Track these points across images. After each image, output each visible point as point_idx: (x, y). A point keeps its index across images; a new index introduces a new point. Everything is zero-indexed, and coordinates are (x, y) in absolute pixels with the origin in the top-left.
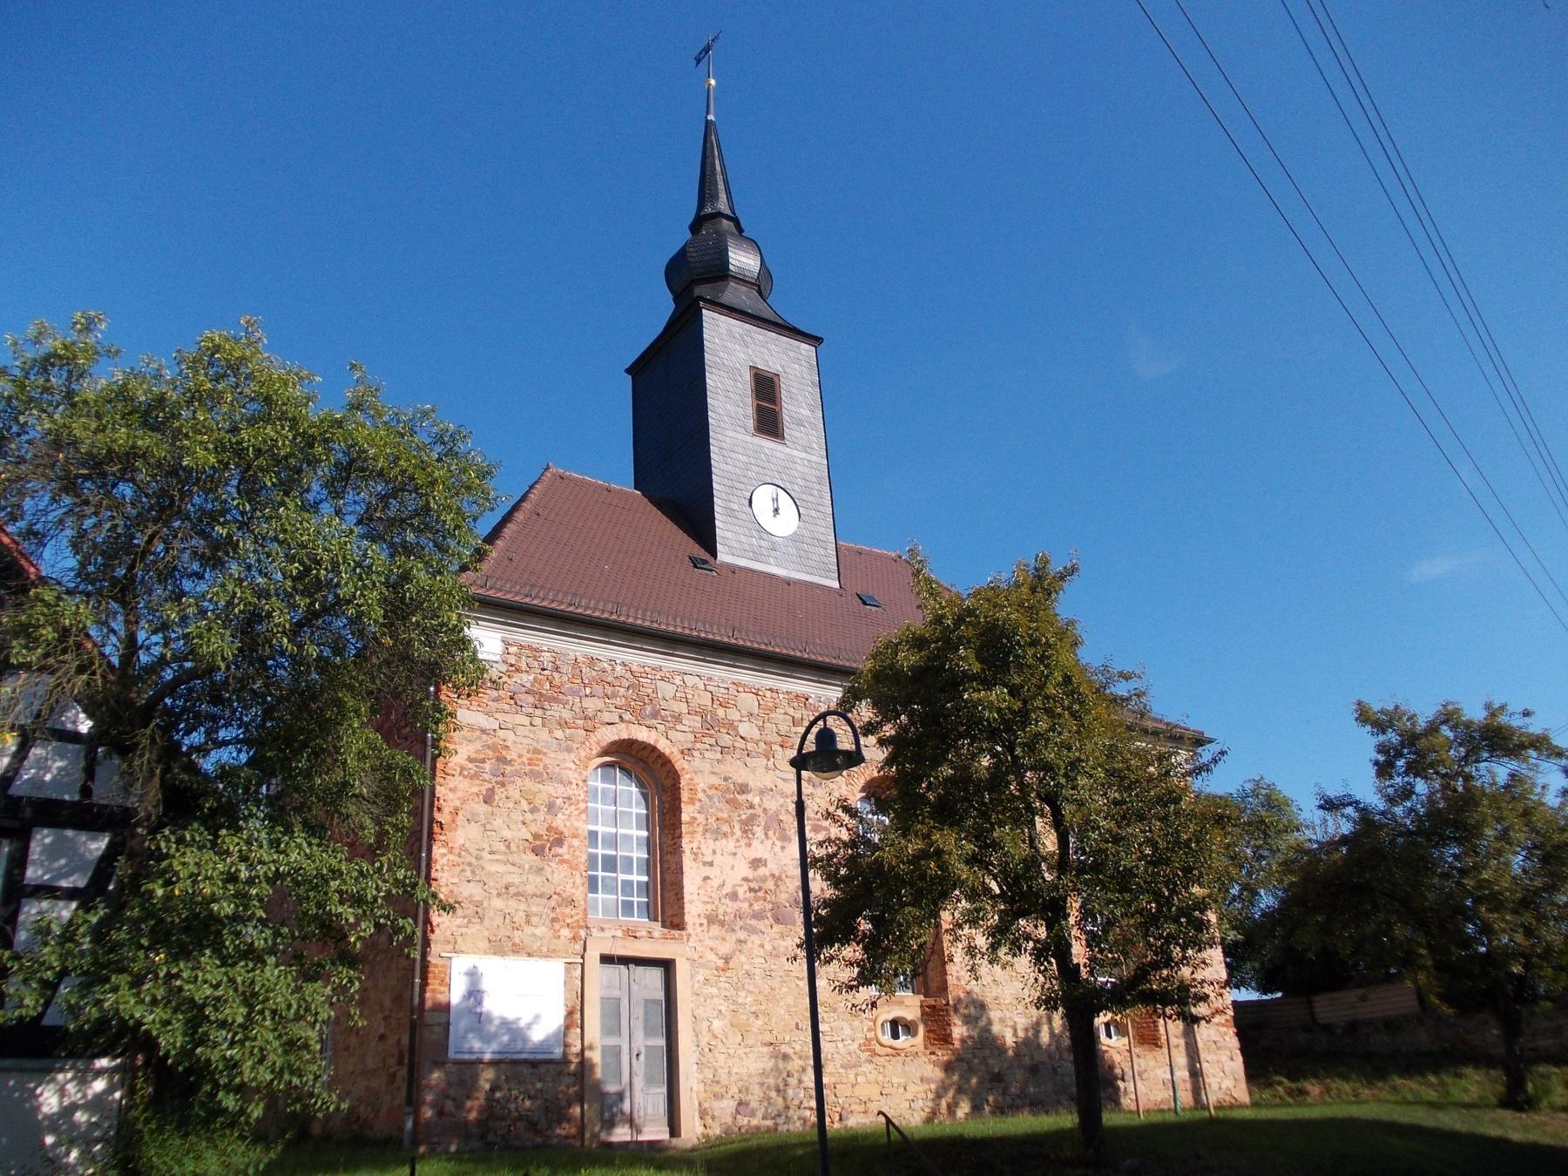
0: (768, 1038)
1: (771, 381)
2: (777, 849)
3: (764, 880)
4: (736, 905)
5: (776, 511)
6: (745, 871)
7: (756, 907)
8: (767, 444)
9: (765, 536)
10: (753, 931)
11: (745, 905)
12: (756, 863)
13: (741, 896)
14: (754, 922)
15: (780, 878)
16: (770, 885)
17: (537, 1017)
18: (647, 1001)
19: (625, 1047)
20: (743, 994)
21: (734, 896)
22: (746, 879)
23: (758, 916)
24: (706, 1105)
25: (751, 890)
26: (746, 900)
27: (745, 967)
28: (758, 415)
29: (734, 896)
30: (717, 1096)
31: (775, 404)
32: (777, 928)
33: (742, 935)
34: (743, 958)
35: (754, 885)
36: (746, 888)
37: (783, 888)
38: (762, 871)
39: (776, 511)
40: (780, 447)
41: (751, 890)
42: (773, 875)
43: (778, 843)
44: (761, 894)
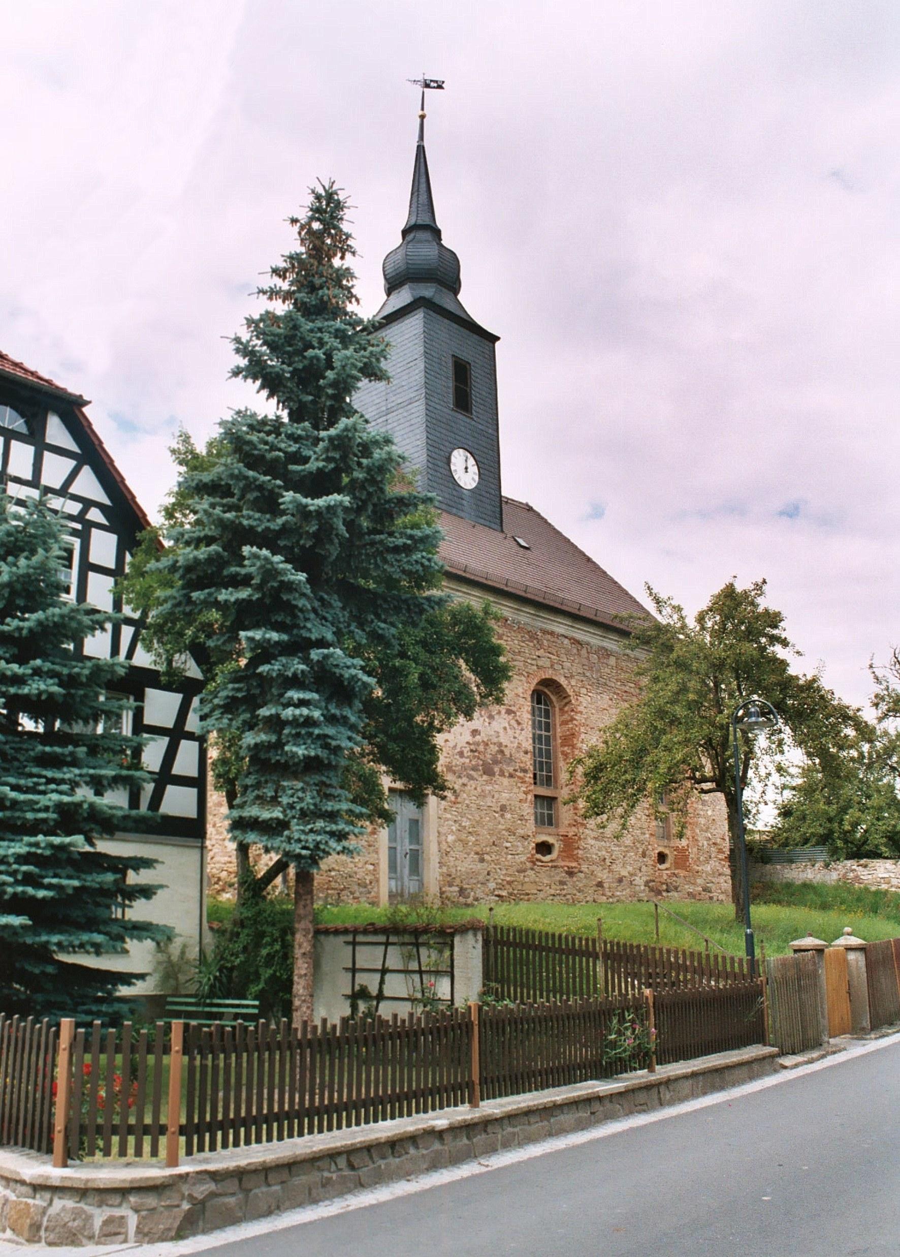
0: (477, 849)
1: (465, 367)
2: (487, 724)
3: (478, 744)
4: (463, 760)
5: (466, 468)
6: (469, 738)
7: (473, 763)
8: (461, 417)
9: (457, 488)
10: (471, 778)
11: (467, 761)
12: (475, 732)
13: (466, 755)
14: (472, 772)
15: (487, 745)
16: (481, 748)
17: (258, 392)
18: (410, 820)
19: (399, 848)
20: (464, 819)
21: (461, 754)
22: (468, 743)
23: (475, 769)
24: (444, 889)
25: (472, 751)
26: (468, 757)
27: (467, 802)
28: (466, 378)
29: (461, 754)
30: (451, 885)
31: (466, 385)
32: (485, 777)
33: (465, 780)
34: (465, 795)
35: (473, 747)
36: (468, 749)
37: (489, 751)
38: (478, 738)
39: (466, 468)
40: (468, 420)
41: (472, 751)
42: (483, 741)
43: (487, 720)
44: (476, 754)
